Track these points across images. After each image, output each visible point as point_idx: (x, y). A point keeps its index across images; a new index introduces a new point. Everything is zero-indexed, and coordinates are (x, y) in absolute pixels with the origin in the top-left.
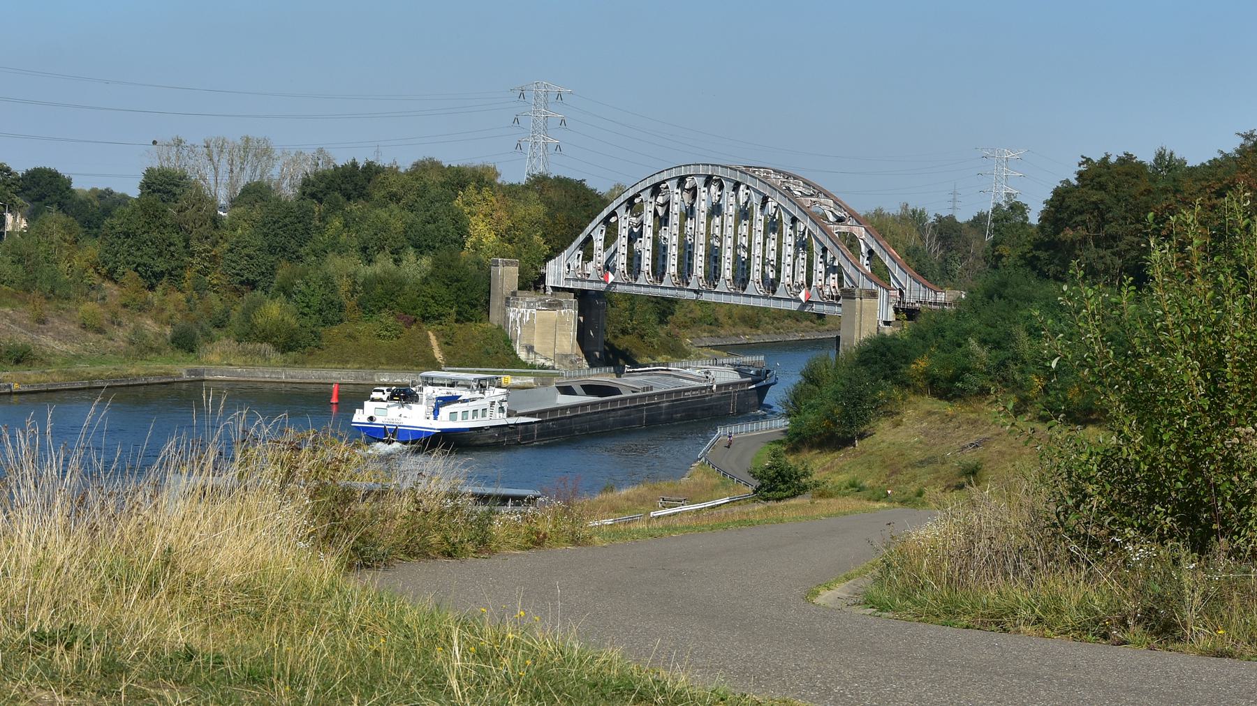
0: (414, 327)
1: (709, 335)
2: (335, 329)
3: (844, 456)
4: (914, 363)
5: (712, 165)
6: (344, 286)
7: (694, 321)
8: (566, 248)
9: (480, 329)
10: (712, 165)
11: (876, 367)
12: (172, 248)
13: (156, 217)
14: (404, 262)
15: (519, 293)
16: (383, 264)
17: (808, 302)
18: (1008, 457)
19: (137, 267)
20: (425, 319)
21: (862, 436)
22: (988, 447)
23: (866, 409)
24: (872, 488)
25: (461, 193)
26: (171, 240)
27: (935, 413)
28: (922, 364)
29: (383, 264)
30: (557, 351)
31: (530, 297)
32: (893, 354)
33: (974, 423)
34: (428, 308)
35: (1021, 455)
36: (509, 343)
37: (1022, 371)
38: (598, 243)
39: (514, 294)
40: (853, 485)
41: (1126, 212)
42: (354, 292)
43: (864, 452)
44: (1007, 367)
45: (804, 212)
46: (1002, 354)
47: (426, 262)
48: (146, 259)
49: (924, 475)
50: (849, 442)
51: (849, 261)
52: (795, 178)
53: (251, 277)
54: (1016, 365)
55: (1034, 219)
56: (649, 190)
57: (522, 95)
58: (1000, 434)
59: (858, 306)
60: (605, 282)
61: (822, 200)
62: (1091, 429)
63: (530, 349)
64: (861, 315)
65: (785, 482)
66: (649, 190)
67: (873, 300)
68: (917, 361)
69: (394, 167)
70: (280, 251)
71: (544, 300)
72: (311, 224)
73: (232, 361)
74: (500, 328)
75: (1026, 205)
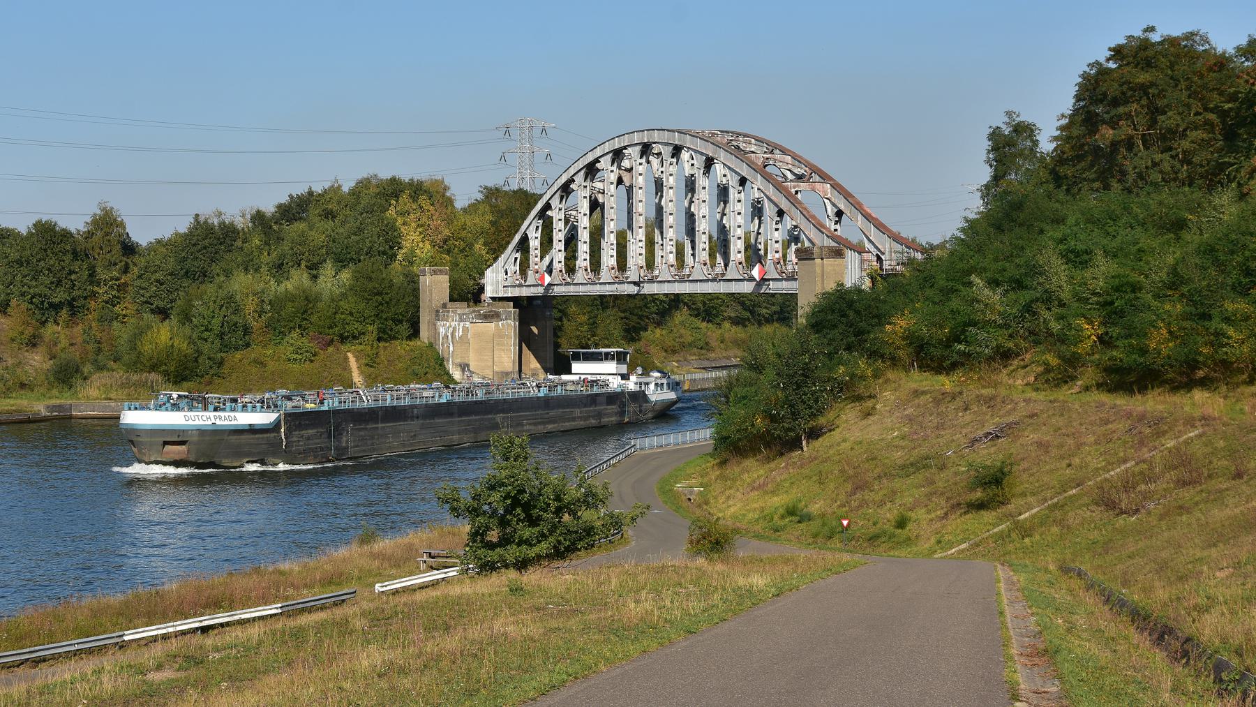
0: (330, 349)
1: (697, 358)
2: (238, 355)
3: (786, 467)
4: (890, 323)
5: (647, 130)
6: (250, 305)
7: (683, 346)
8: (502, 253)
9: (408, 348)
10: (647, 130)
11: (835, 333)
12: (73, 277)
13: (54, 243)
14: (322, 277)
15: (449, 305)
16: (297, 280)
17: (763, 280)
18: (1054, 452)
19: (31, 299)
20: (343, 339)
21: (814, 434)
22: (1018, 437)
23: (815, 392)
24: (823, 515)
25: (393, 202)
26: (72, 268)
27: (924, 393)
28: (900, 324)
29: (297, 280)
30: (496, 369)
31: (461, 308)
32: (858, 312)
33: (989, 401)
34: (346, 326)
35: (1079, 446)
36: (440, 362)
37: (1061, 318)
38: (534, 243)
39: (444, 306)
40: (791, 512)
41: (1189, 97)
42: (261, 312)
43: (815, 458)
44: (1034, 314)
45: (754, 169)
46: (1025, 296)
47: (345, 275)
48: (42, 290)
49: (910, 490)
50: (795, 444)
51: (810, 221)
52: (745, 136)
53: (162, 304)
54: (1049, 309)
55: (1046, 145)
56: (582, 172)
57: (507, 132)
58: (1036, 415)
59: (818, 270)
60: (542, 285)
61: (777, 157)
62: (1199, 395)
63: (464, 367)
64: (823, 281)
65: (533, 522)
66: (583, 172)
67: (839, 261)
68: (894, 320)
69: (336, 185)
70: (199, 276)
71: (479, 311)
72: (232, 245)
73: (113, 395)
74: (431, 345)
75: (1034, 125)
